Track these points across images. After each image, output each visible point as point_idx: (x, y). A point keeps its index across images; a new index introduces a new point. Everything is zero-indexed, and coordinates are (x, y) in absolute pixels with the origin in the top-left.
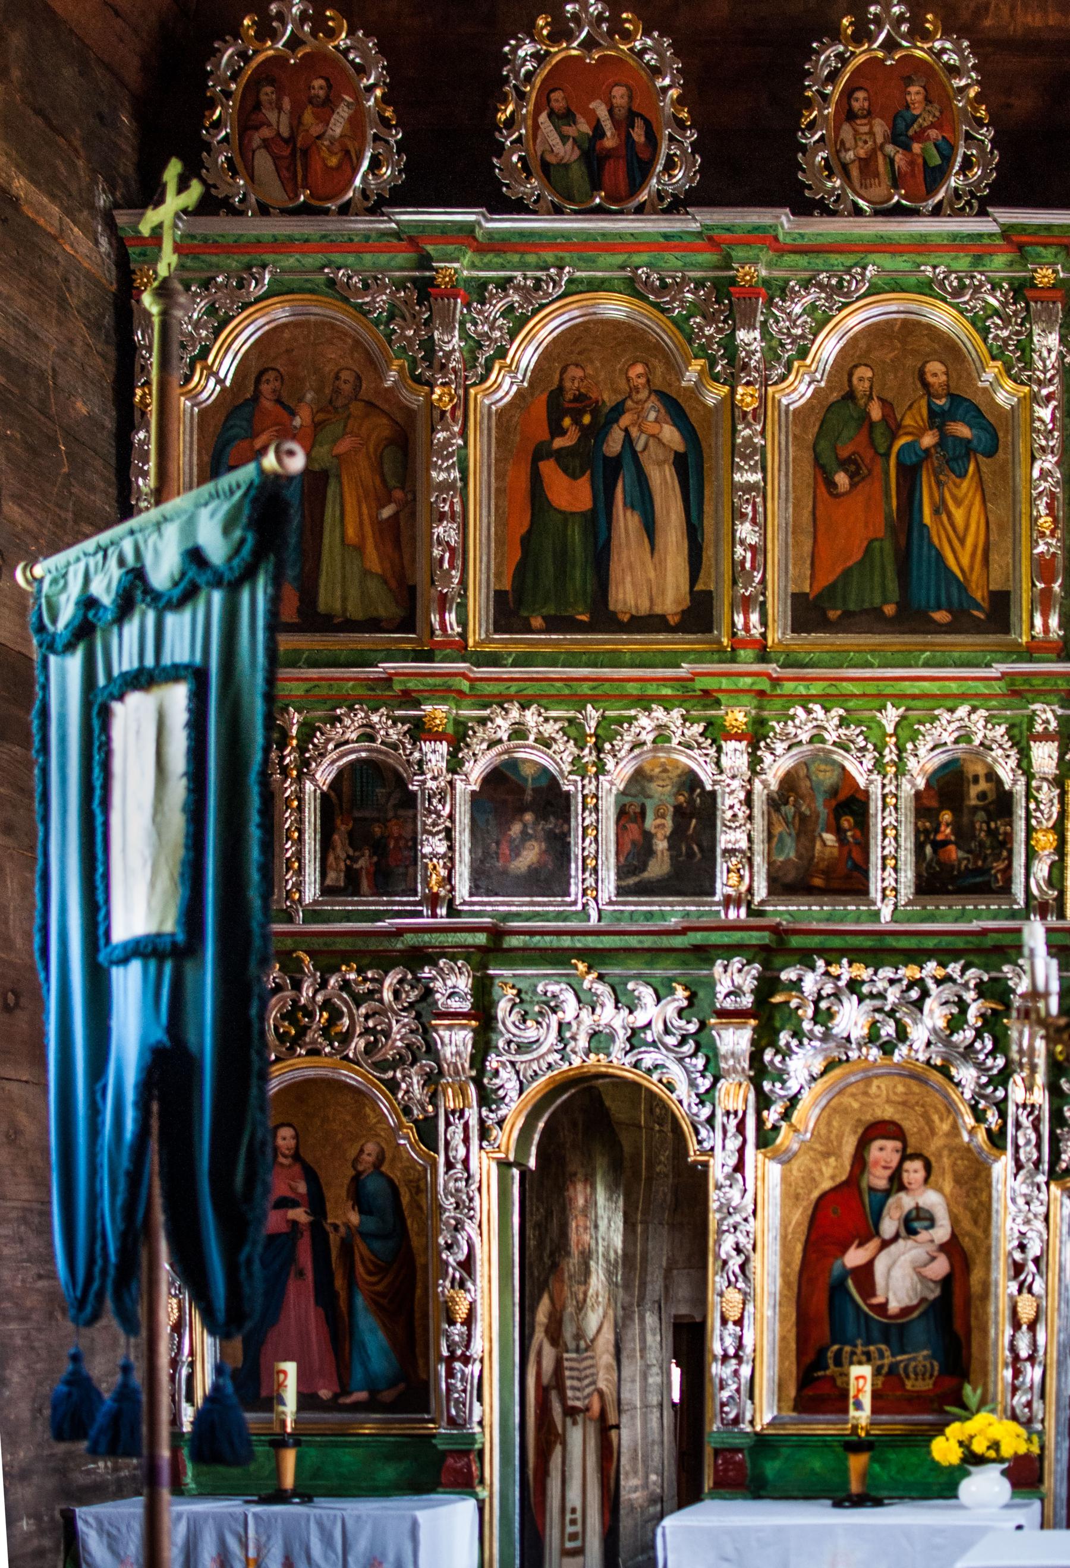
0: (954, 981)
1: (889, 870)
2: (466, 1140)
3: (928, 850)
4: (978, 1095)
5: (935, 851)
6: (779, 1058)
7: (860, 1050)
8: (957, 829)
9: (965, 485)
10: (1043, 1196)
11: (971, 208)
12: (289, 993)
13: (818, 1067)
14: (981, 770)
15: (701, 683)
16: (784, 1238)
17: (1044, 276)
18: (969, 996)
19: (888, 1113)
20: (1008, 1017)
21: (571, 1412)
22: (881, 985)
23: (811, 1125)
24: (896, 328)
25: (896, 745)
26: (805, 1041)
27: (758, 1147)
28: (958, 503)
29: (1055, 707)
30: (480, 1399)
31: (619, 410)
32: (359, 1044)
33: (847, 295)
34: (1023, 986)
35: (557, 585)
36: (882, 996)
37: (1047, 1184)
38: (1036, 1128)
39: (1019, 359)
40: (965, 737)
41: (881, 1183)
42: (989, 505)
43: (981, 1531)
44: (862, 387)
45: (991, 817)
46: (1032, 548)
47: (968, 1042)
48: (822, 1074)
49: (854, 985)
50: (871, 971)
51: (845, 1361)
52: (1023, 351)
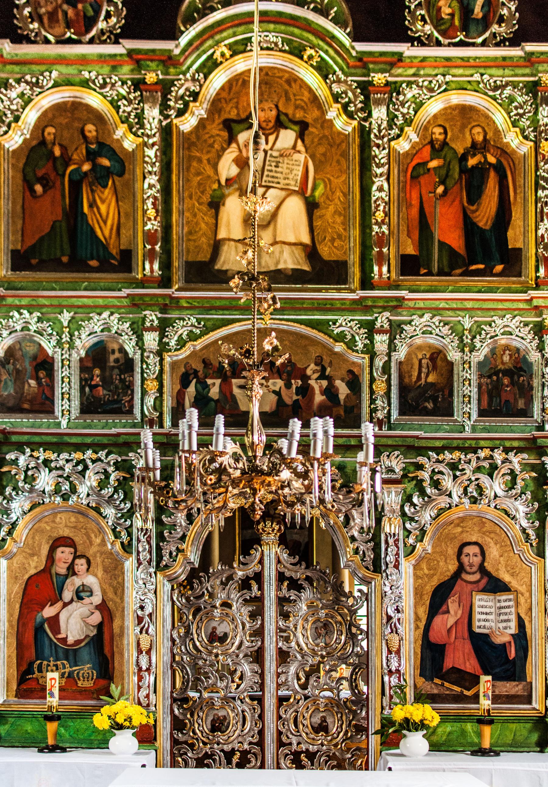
0: (102, 461)
1: (66, 400)
3: (87, 389)
5: (91, 390)
6: (5, 501)
7: (50, 498)
8: (103, 378)
9: (107, 191)
10: (153, 580)
11: (110, 39)
13: (27, 507)
14: (116, 347)
16: (9, 600)
17: (151, 78)
18: (111, 469)
19: (66, 533)
20: (133, 481)
22: (61, 463)
23: (24, 539)
24: (69, 106)
25: (69, 332)
26: (20, 493)
28: (103, 201)
29: (157, 313)
33: (42, 87)
34: (141, 463)
36: (62, 468)
37: (155, 573)
38: (149, 543)
39: (137, 123)
40: (107, 328)
42: (120, 203)
43: (123, 767)
45: (122, 372)
46: (144, 226)
47: (110, 494)
48: (29, 511)
49: (46, 463)
50: (56, 455)
51: (44, 670)
52: (139, 119)
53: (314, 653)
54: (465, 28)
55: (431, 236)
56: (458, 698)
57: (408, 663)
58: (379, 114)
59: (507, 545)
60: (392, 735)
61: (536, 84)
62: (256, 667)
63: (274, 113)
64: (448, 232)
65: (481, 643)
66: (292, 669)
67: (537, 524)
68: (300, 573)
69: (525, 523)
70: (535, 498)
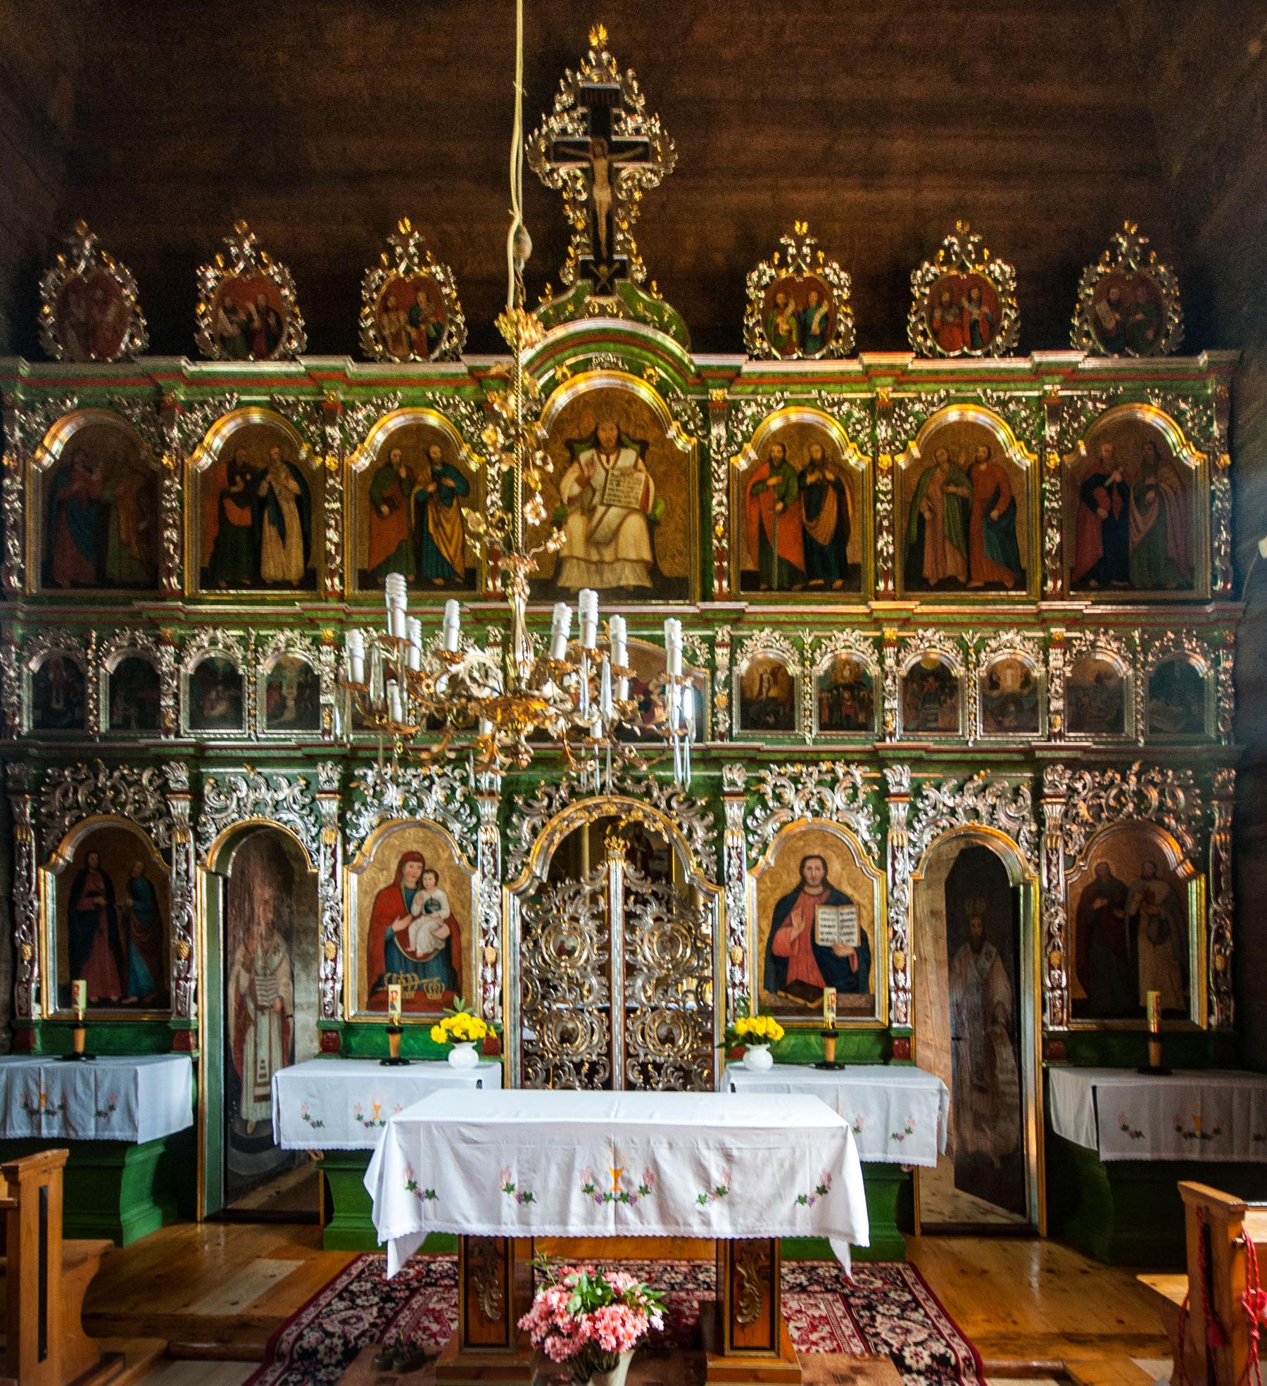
4: (462, 837)
12: (92, 781)
13: (375, 822)
18: (457, 784)
19: (415, 847)
21: (260, 1009)
22: (409, 777)
28: (448, 521)
30: (196, 1000)
31: (265, 472)
35: (233, 562)
36: (409, 784)
54: (803, 345)
57: (751, 977)
58: (718, 431)
59: (848, 856)
60: (737, 1046)
61: (872, 400)
62: (604, 980)
63: (615, 433)
64: (788, 548)
65: (824, 956)
66: (639, 982)
67: (879, 837)
68: (646, 888)
69: (867, 837)
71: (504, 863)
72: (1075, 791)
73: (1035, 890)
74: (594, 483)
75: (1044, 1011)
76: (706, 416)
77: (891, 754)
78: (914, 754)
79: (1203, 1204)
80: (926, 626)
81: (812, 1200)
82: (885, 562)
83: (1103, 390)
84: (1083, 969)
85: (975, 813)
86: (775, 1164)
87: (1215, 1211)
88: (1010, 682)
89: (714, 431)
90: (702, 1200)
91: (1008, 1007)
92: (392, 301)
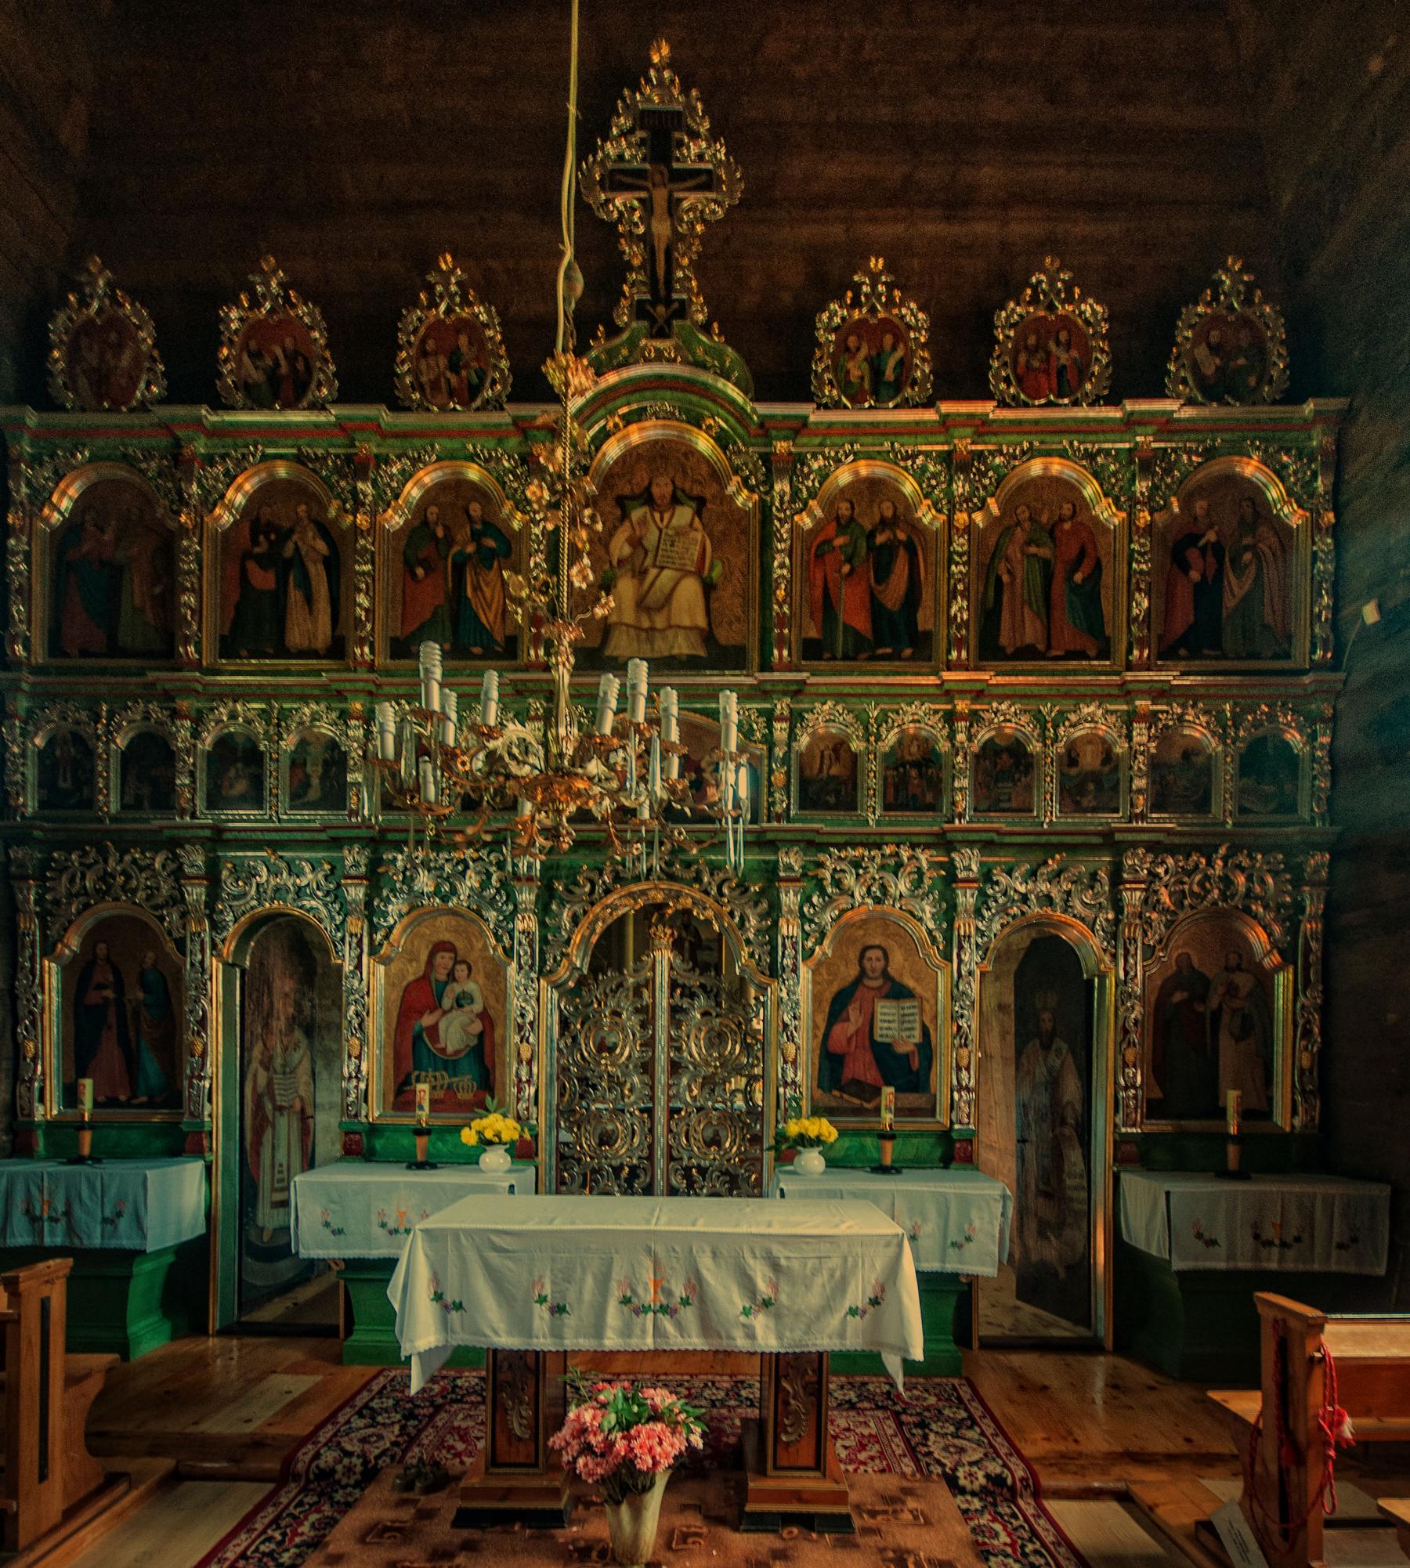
2: (203, 951)
4: (498, 925)
12: (101, 866)
13: (405, 910)
15: (335, 686)
18: (493, 869)
19: (446, 936)
21: (280, 1109)
27: (370, 954)
31: (291, 531)
32: (141, 895)
35: (256, 629)
36: (442, 868)
38: (531, 946)
41: (443, 977)
44: (432, 518)
53: (707, 1064)
54: (875, 392)
55: (836, 619)
56: (858, 1111)
58: (781, 486)
60: (788, 1149)
61: (949, 453)
62: (646, 1079)
63: (670, 488)
64: (854, 615)
65: (884, 1056)
68: (694, 981)
69: (931, 925)
70: (942, 898)
71: (542, 953)
72: (1157, 876)
73: (1111, 982)
74: (646, 543)
75: (1116, 1111)
76: (769, 470)
77: (959, 837)
78: (985, 836)
79: (1279, 1316)
80: (1002, 698)
81: (864, 1312)
82: (959, 628)
83: (1200, 442)
84: (1159, 1068)
85: (1048, 900)
86: (825, 1273)
87: (1293, 1323)
88: (1090, 760)
89: (777, 487)
90: (746, 1312)
91: (1078, 1107)
92: (431, 345)
